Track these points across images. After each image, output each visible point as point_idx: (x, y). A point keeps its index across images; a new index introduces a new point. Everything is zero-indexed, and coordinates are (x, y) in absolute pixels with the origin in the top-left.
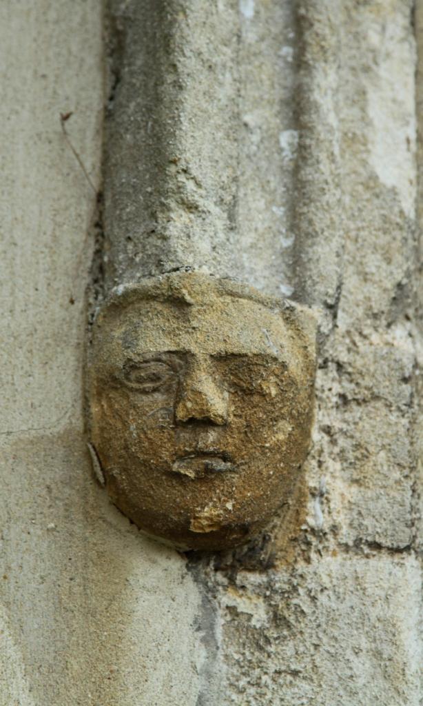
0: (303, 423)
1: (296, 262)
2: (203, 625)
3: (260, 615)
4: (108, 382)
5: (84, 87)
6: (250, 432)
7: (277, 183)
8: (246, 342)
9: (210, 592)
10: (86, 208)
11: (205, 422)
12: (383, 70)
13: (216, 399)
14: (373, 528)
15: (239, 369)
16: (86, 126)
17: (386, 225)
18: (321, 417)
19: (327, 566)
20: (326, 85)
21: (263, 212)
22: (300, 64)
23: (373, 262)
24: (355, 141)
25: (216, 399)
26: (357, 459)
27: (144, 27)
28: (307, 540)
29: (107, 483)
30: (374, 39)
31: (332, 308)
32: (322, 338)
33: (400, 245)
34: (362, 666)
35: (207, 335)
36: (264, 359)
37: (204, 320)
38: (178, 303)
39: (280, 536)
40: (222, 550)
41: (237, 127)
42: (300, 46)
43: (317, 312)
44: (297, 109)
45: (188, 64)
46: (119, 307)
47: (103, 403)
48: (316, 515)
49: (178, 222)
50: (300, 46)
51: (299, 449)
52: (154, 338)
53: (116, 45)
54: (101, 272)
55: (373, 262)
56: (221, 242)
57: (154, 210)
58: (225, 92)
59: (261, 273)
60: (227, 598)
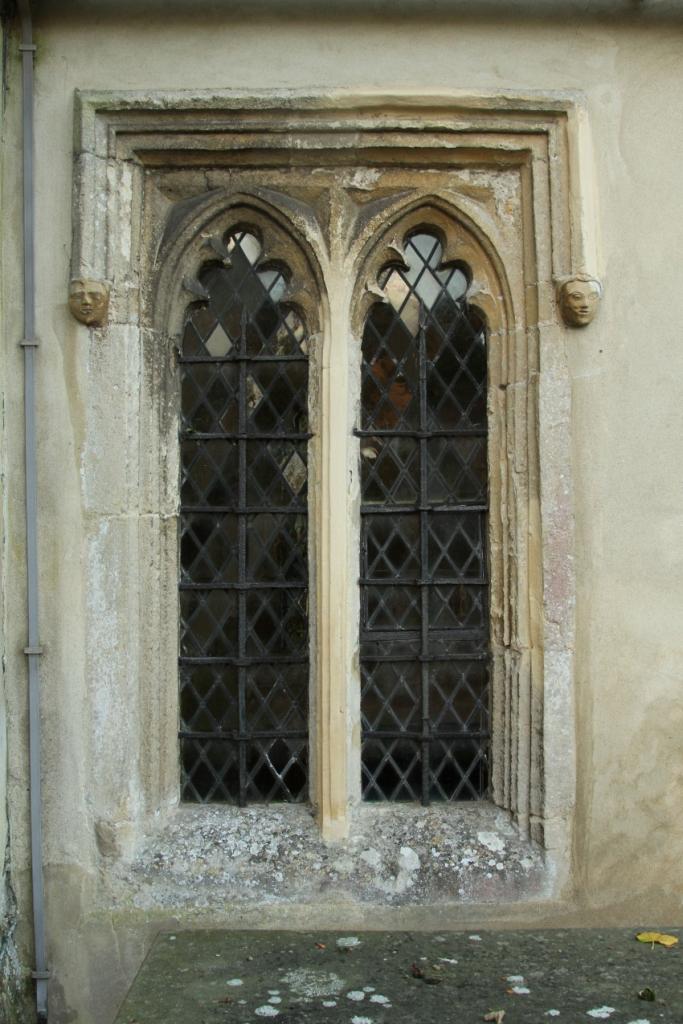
0: (107, 302)
1: (106, 272)
2: (91, 337)
3: (100, 335)
4: (72, 296)
5: (68, 239)
6: (96, 306)
7: (103, 257)
8: (94, 290)
9: (91, 332)
10: (68, 262)
11: (86, 304)
12: (124, 233)
13: (89, 300)
14: (120, 320)
15: (93, 295)
16: (69, 246)
17: (124, 263)
18: (111, 299)
19: (112, 326)
20: (112, 237)
21: (99, 263)
22: (107, 234)
23: (121, 270)
24: (118, 247)
25: (89, 300)
26: (117, 307)
27: (94, 225)
28: (108, 322)
29: (72, 313)
30: (122, 227)
31: (113, 281)
32: (110, 286)
33: (39, 1010)
34: (117, 344)
35: (88, 288)
36: (97, 293)
37: (87, 287)
38: (82, 284)
39: (104, 321)
40: (93, 325)
41: (94, 247)
42: (107, 230)
43: (110, 282)
44: (107, 243)
45: (83, 238)
46: (74, 282)
47: (147, 186)
48: (110, 318)
49: (82, 268)
50: (107, 230)
51: (106, 307)
52: (78, 290)
53: (73, 232)
54: (71, 275)
55: (121, 270)
56: (91, 272)
57: (79, 265)
58: (91, 242)
59: (99, 275)
60: (94, 332)
